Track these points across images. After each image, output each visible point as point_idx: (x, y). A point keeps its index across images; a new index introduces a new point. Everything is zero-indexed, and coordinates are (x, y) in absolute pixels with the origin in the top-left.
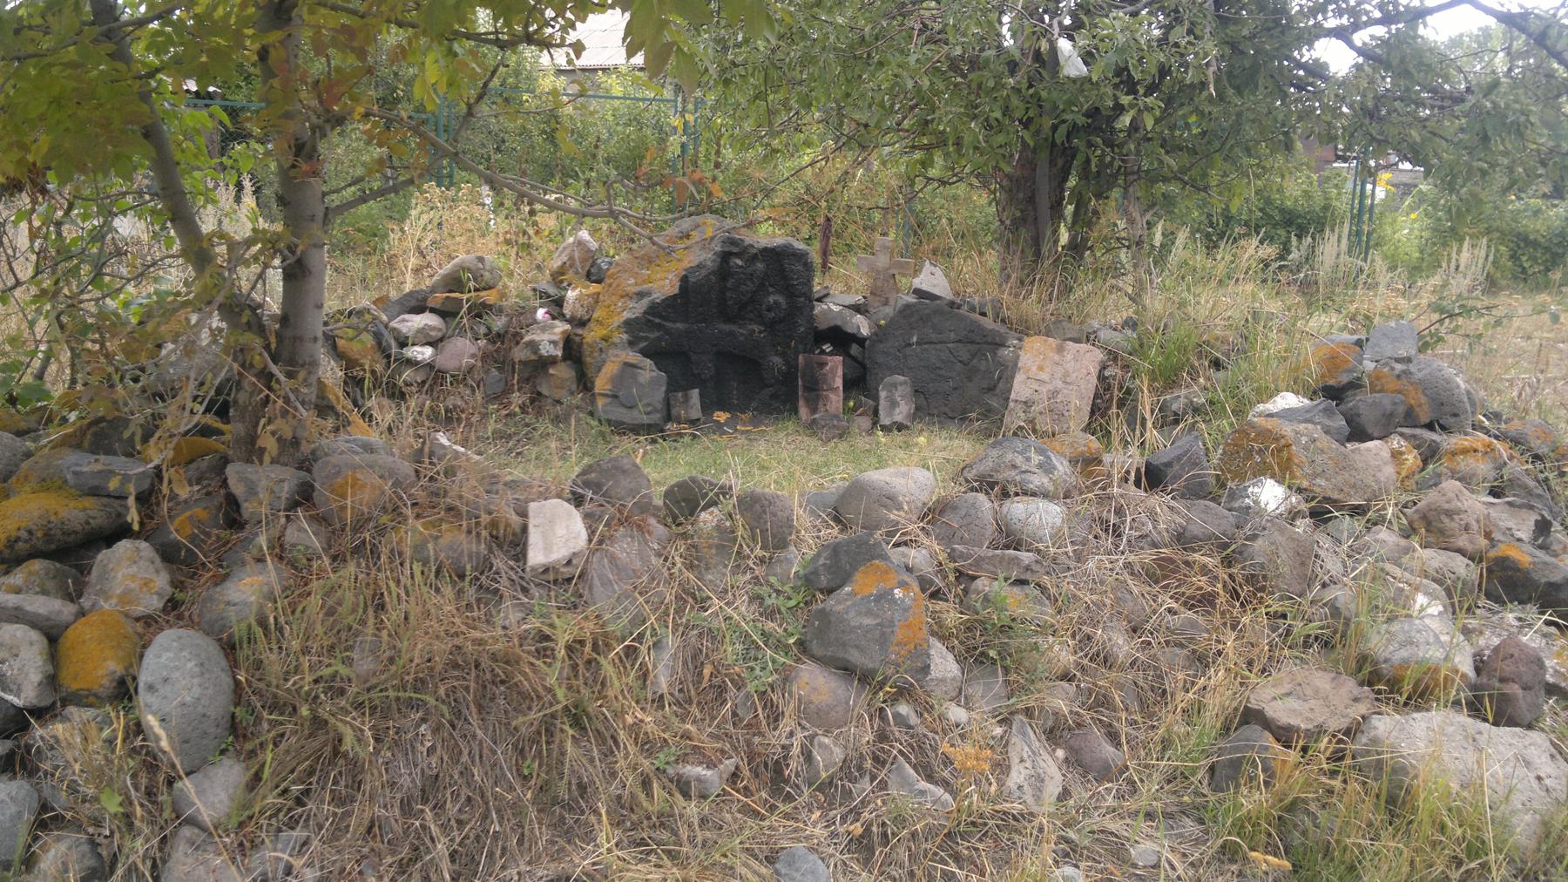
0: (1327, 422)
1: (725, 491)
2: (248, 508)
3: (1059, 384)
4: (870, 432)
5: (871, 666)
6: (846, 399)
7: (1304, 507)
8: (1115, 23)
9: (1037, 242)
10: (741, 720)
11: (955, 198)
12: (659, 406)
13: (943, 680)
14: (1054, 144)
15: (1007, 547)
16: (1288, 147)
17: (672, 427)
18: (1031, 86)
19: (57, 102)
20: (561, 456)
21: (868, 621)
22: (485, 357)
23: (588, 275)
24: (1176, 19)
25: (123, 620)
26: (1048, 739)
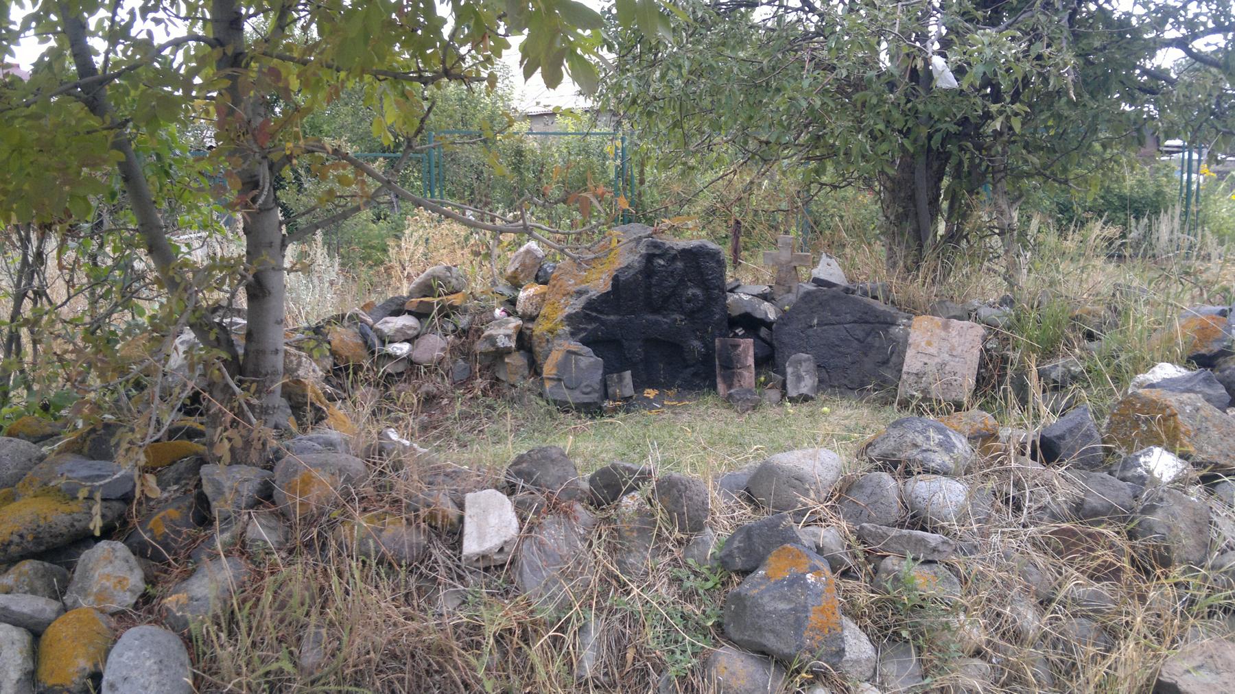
1: (645, 476)
2: (217, 508)
3: (946, 357)
4: (780, 403)
5: (786, 651)
6: (758, 375)
7: (1196, 475)
12: (597, 387)
13: (858, 661)
14: (929, 149)
17: (608, 404)
18: (909, 101)
21: (783, 606)
22: (453, 349)
25: (98, 616)
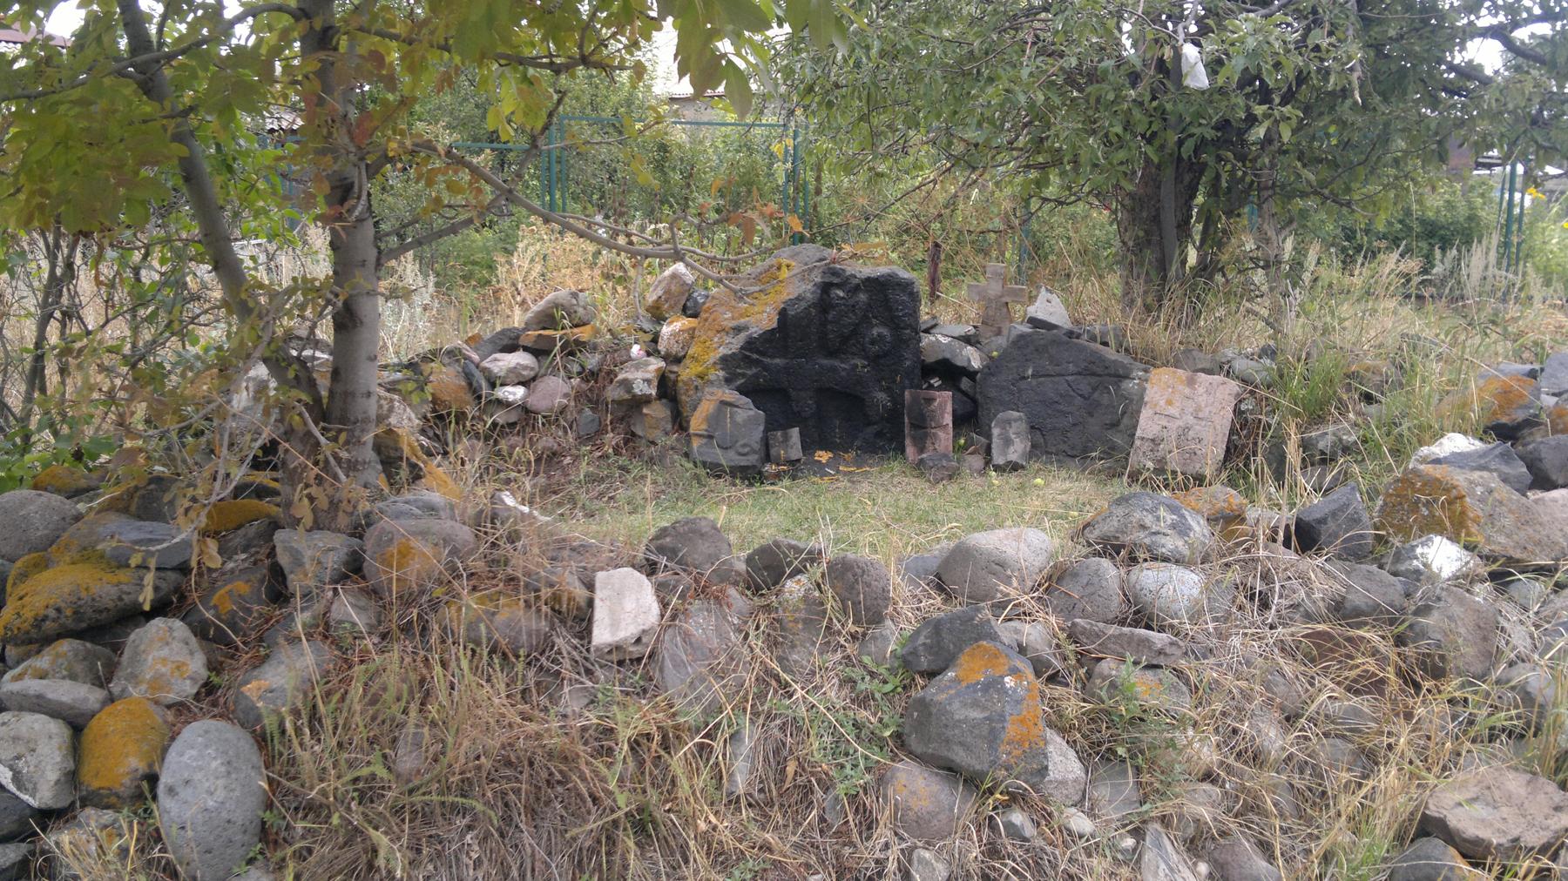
0: (1506, 469)
1: (814, 557)
2: (296, 583)
3: (1191, 420)
4: (983, 472)
5: (978, 767)
6: (956, 436)
7: (1484, 571)
8: (1245, 24)
9: (1162, 265)
10: (830, 827)
11: (1073, 217)
12: (757, 447)
14: (1180, 158)
15: (1136, 624)
16: (1442, 158)
17: (770, 468)
18: (1154, 98)
19: (63, 143)
20: (642, 514)
21: (976, 714)
23: (684, 310)
24: (1314, 22)
26: (1189, 850)
